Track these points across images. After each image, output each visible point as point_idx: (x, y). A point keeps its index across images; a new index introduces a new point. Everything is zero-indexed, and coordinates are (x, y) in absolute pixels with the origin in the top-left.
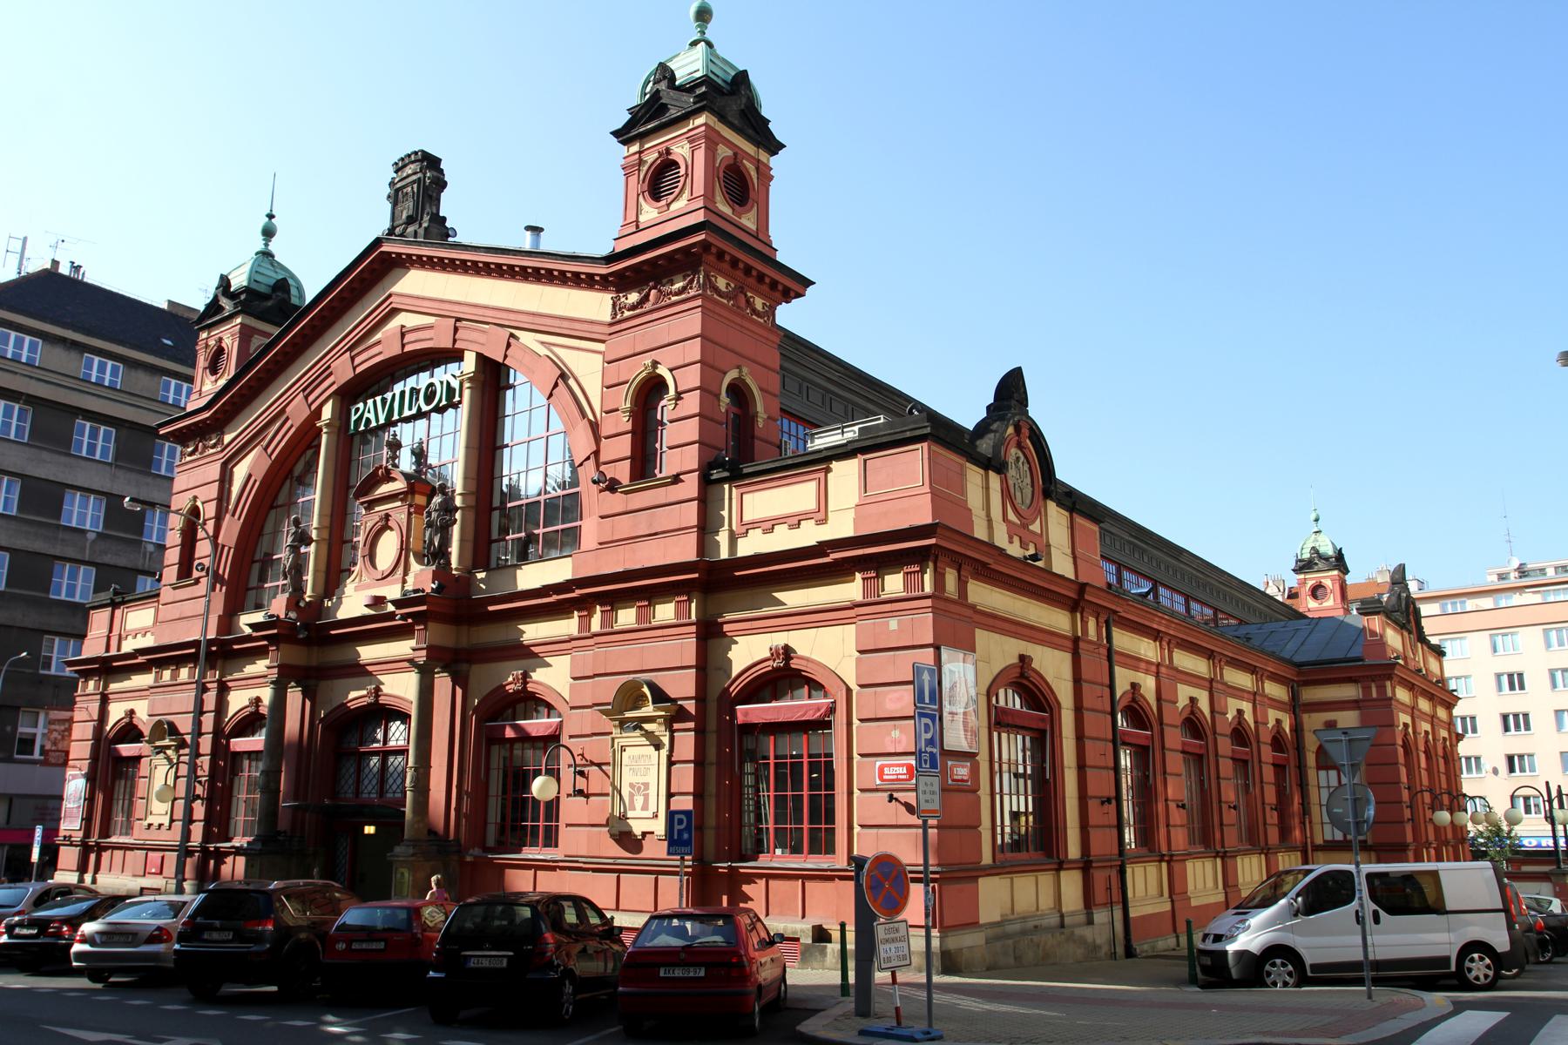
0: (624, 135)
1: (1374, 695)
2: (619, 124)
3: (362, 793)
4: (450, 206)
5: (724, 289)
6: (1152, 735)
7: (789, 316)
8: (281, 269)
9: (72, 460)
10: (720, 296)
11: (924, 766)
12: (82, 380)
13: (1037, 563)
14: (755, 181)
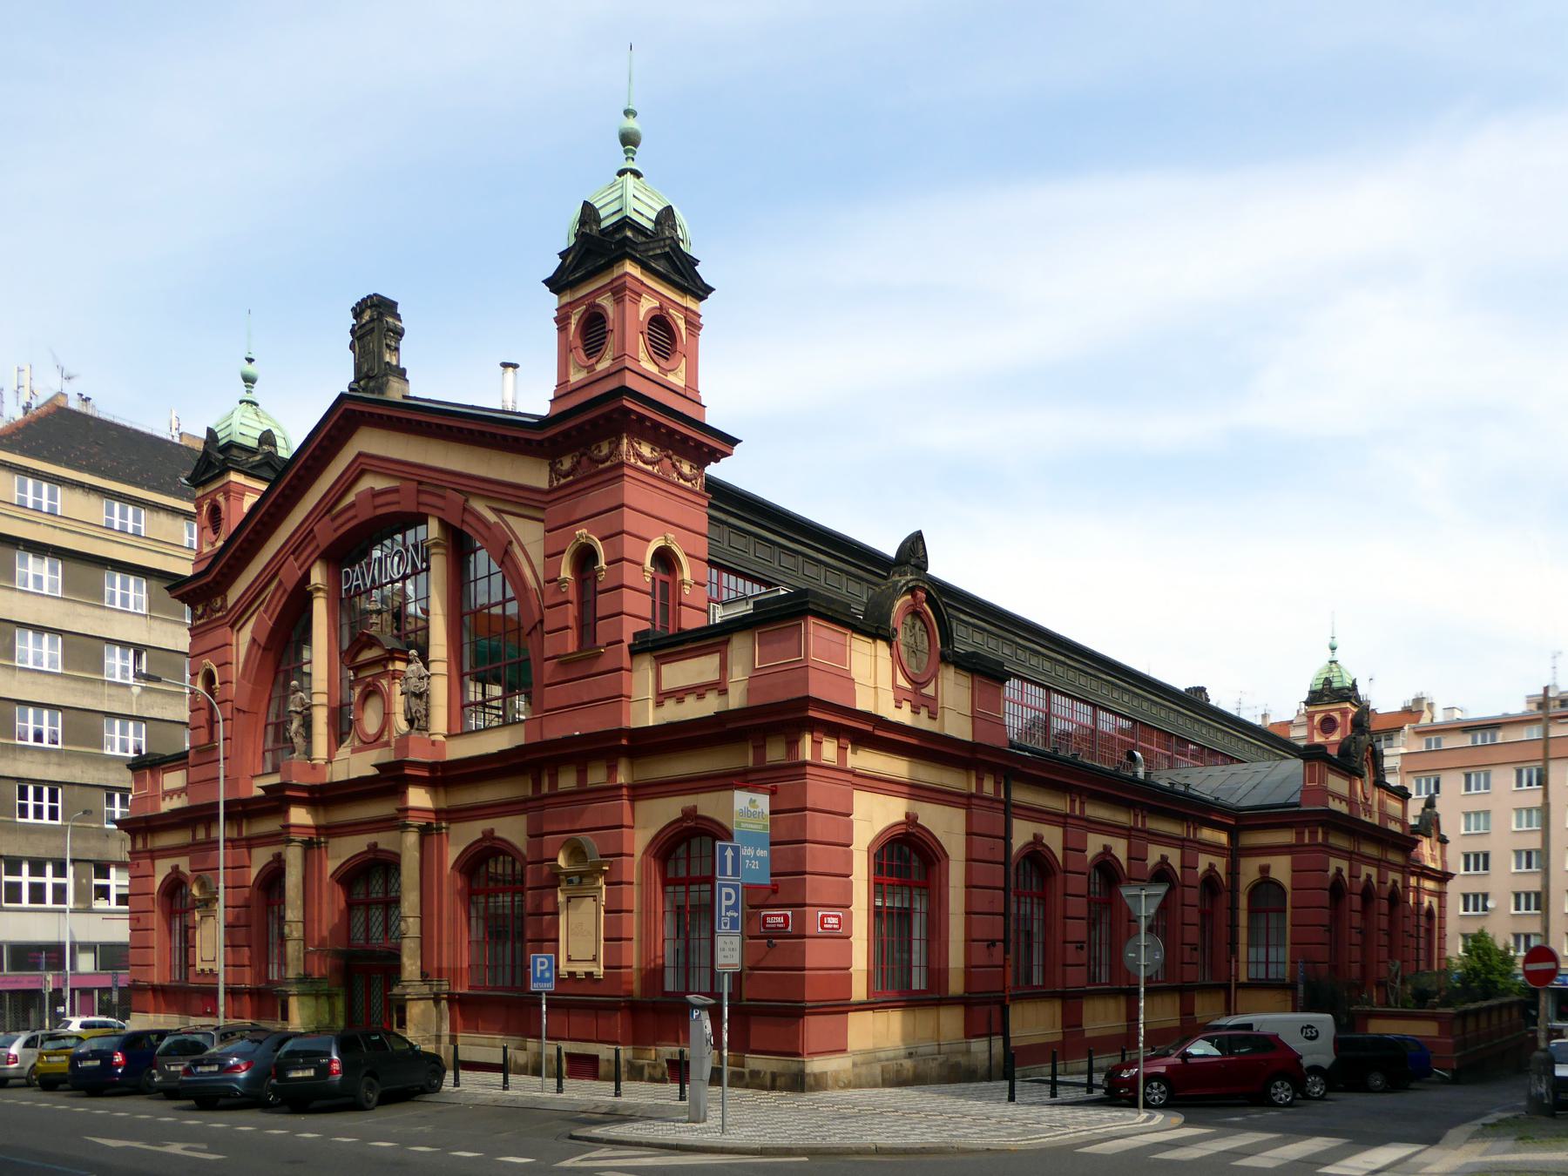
0: (555, 284)
1: (1307, 841)
2: (549, 272)
3: (371, 939)
4: (409, 355)
7: (713, 470)
8: (267, 419)
9: (106, 613)
11: (723, 927)
12: (106, 528)
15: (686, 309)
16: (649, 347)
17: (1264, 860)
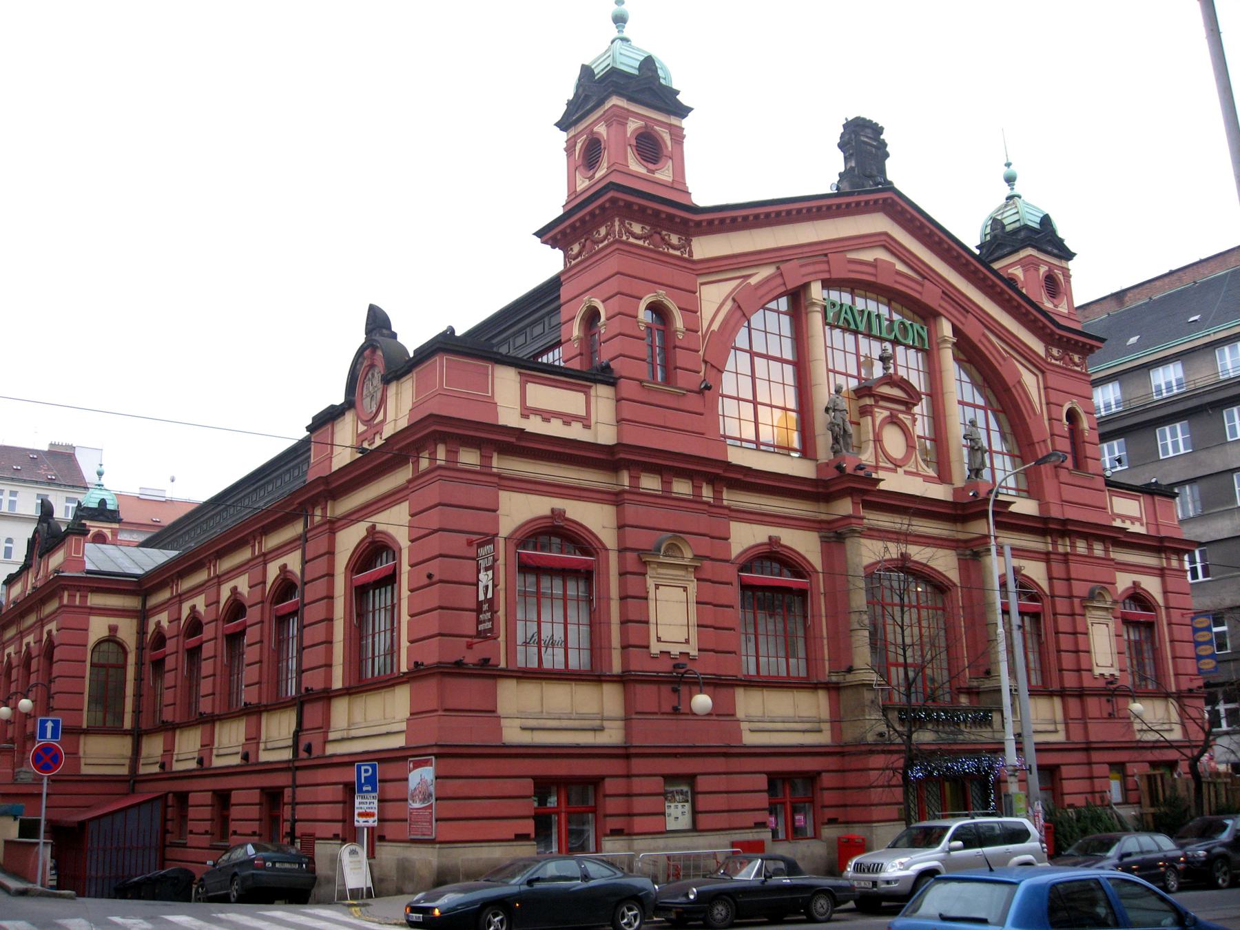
0: (563, 125)
2: (558, 117)
10: (1056, 360)
14: (1063, 281)
15: (670, 125)
17: (113, 621)
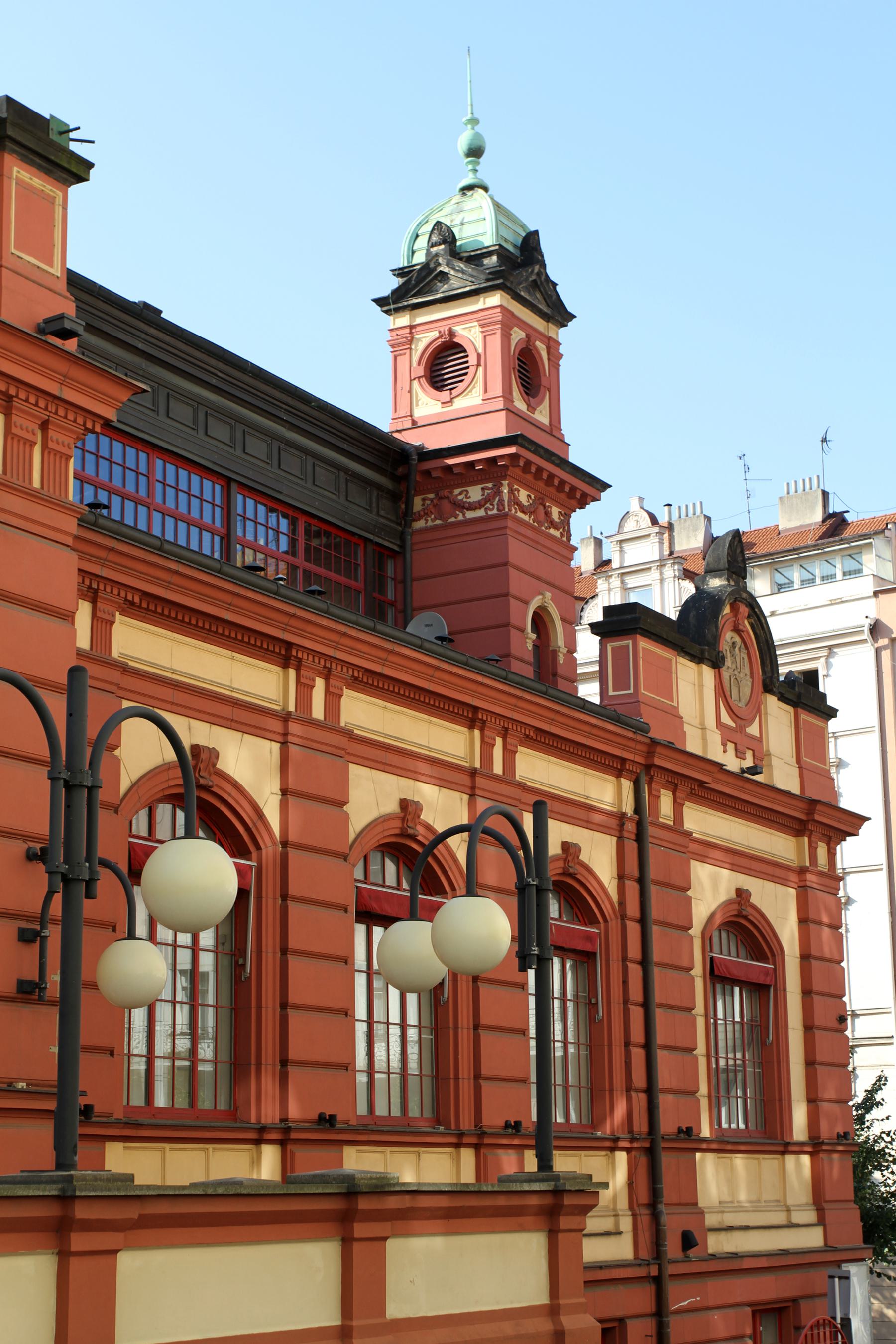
5: (526, 504)
6: (775, 969)
13: (756, 777)
16: (520, 385)
